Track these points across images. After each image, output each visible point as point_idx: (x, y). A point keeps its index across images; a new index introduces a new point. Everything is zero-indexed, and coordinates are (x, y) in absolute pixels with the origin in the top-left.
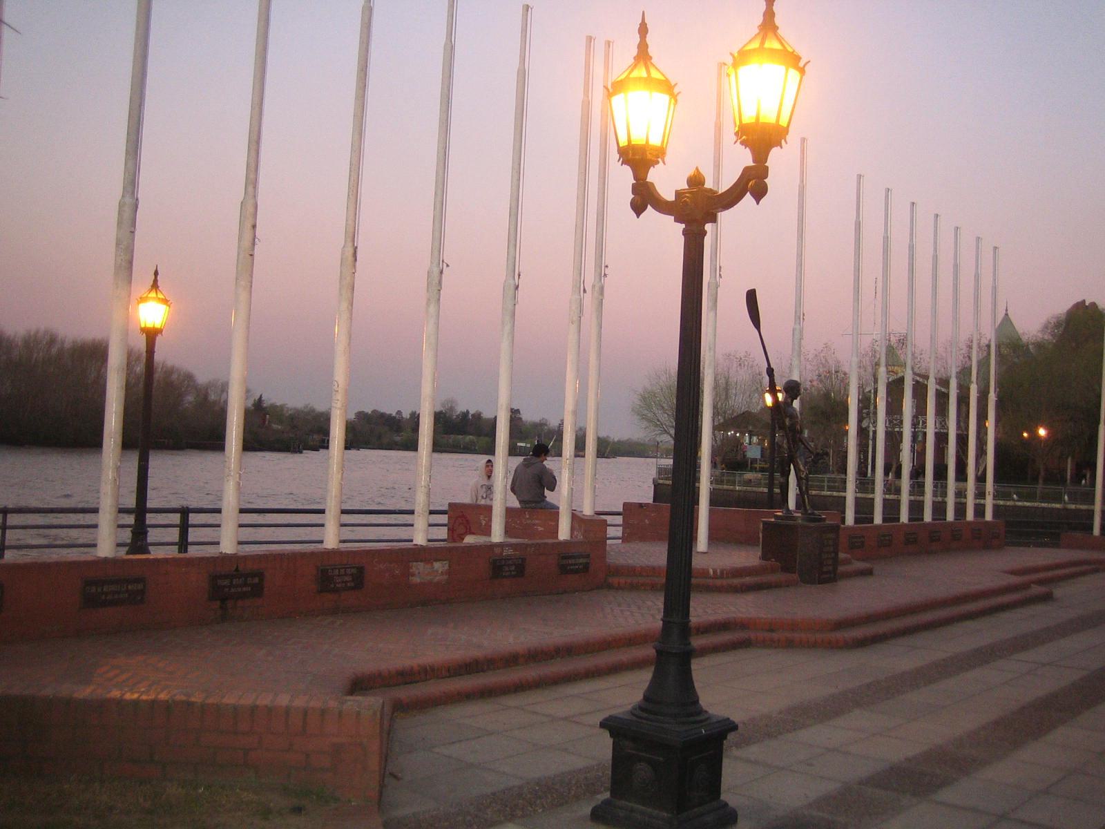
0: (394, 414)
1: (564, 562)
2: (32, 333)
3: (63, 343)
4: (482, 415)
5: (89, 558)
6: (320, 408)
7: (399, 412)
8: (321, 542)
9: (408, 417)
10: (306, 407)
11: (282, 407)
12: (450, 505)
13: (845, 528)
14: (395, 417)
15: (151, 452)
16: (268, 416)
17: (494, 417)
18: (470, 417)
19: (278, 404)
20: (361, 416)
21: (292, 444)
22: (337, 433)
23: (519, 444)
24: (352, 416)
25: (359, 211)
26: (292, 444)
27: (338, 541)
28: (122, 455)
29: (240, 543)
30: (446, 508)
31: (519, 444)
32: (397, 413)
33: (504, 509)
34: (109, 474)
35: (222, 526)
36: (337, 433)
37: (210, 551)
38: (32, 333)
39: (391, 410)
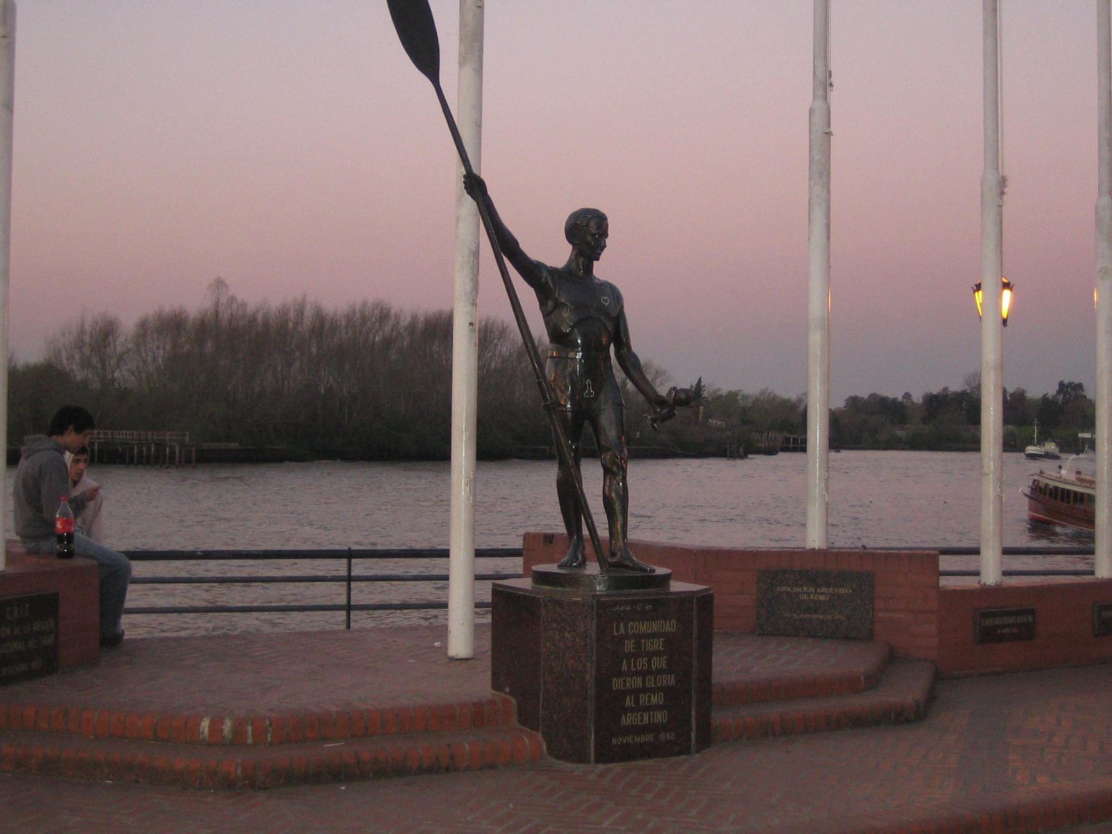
0: (900, 399)
1: (988, 622)
2: (357, 308)
3: (397, 318)
4: (1026, 395)
5: (976, 585)
6: (787, 392)
7: (907, 396)
8: (977, 574)
9: (920, 401)
10: (763, 393)
11: (732, 396)
12: (527, 537)
13: (1095, 584)
14: (901, 403)
15: (582, 459)
16: (701, 407)
17: (695, 383)
18: (1009, 398)
19: (935, 393)
20: (854, 402)
21: (728, 446)
22: (817, 432)
23: (1080, 435)
24: (839, 403)
25: (1002, 135)
26: (728, 446)
27: (1000, 573)
28: (477, 467)
29: (1005, 573)
30: (518, 544)
31: (1080, 435)
32: (904, 397)
33: (474, 550)
34: (990, 489)
35: (983, 551)
36: (817, 432)
37: (969, 583)
38: (357, 308)
39: (893, 392)
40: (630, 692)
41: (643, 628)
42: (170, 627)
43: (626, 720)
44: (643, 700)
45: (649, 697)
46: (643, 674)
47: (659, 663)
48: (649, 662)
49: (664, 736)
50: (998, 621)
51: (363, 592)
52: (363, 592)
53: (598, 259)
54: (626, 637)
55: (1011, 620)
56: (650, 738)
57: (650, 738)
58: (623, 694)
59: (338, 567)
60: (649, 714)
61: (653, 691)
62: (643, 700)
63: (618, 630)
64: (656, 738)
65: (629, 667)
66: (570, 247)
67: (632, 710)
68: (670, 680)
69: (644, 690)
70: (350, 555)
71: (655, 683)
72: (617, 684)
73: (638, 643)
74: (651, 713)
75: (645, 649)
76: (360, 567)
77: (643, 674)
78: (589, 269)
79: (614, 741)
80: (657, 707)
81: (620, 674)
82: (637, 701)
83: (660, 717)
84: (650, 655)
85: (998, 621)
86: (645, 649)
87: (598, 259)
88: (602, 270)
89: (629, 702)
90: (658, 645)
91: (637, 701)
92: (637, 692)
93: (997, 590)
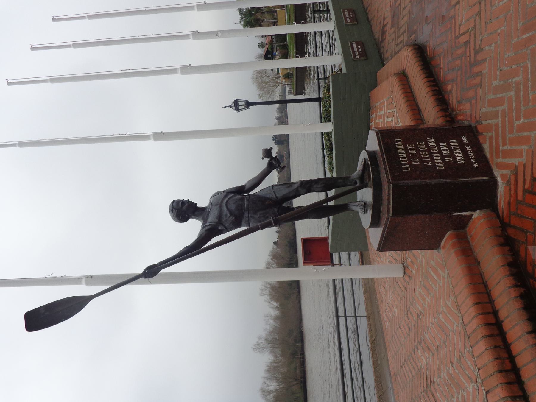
40: (443, 160)
41: (403, 156)
42: (332, 329)
43: (461, 160)
44: (446, 153)
45: (444, 150)
46: (431, 154)
47: (421, 146)
48: (423, 151)
49: (465, 139)
50: (357, 53)
51: (350, 312)
52: (350, 312)
53: (196, 204)
54: (410, 164)
55: (355, 49)
56: (468, 149)
57: (468, 149)
58: (446, 164)
59: (342, 320)
60: (454, 149)
61: (439, 148)
62: (446, 153)
63: (407, 169)
64: (467, 145)
65: (429, 161)
66: (191, 220)
67: (454, 158)
68: (431, 141)
69: (440, 152)
70: (337, 316)
71: (435, 147)
72: (440, 167)
73: (413, 157)
74: (453, 148)
75: (415, 154)
76: (341, 313)
77: (431, 154)
78: (203, 209)
79: (476, 166)
80: (449, 145)
81: (434, 166)
82: (448, 156)
83: (454, 143)
84: (418, 151)
85: (357, 53)
86: (415, 154)
87: (196, 204)
88: (203, 202)
89: (450, 160)
90: (412, 150)
91: (448, 156)
92: (443, 157)
93: (335, 125)
